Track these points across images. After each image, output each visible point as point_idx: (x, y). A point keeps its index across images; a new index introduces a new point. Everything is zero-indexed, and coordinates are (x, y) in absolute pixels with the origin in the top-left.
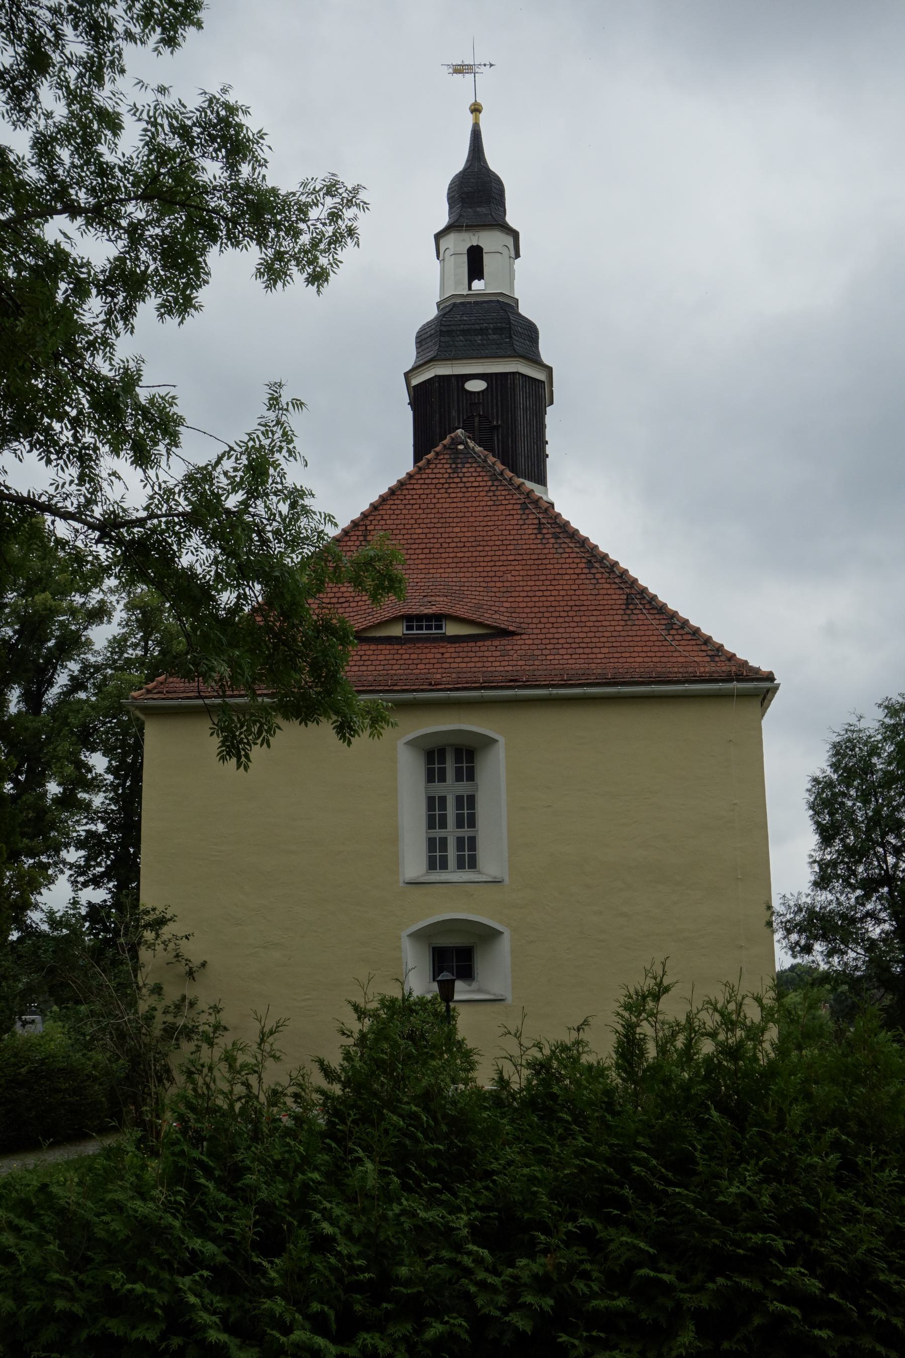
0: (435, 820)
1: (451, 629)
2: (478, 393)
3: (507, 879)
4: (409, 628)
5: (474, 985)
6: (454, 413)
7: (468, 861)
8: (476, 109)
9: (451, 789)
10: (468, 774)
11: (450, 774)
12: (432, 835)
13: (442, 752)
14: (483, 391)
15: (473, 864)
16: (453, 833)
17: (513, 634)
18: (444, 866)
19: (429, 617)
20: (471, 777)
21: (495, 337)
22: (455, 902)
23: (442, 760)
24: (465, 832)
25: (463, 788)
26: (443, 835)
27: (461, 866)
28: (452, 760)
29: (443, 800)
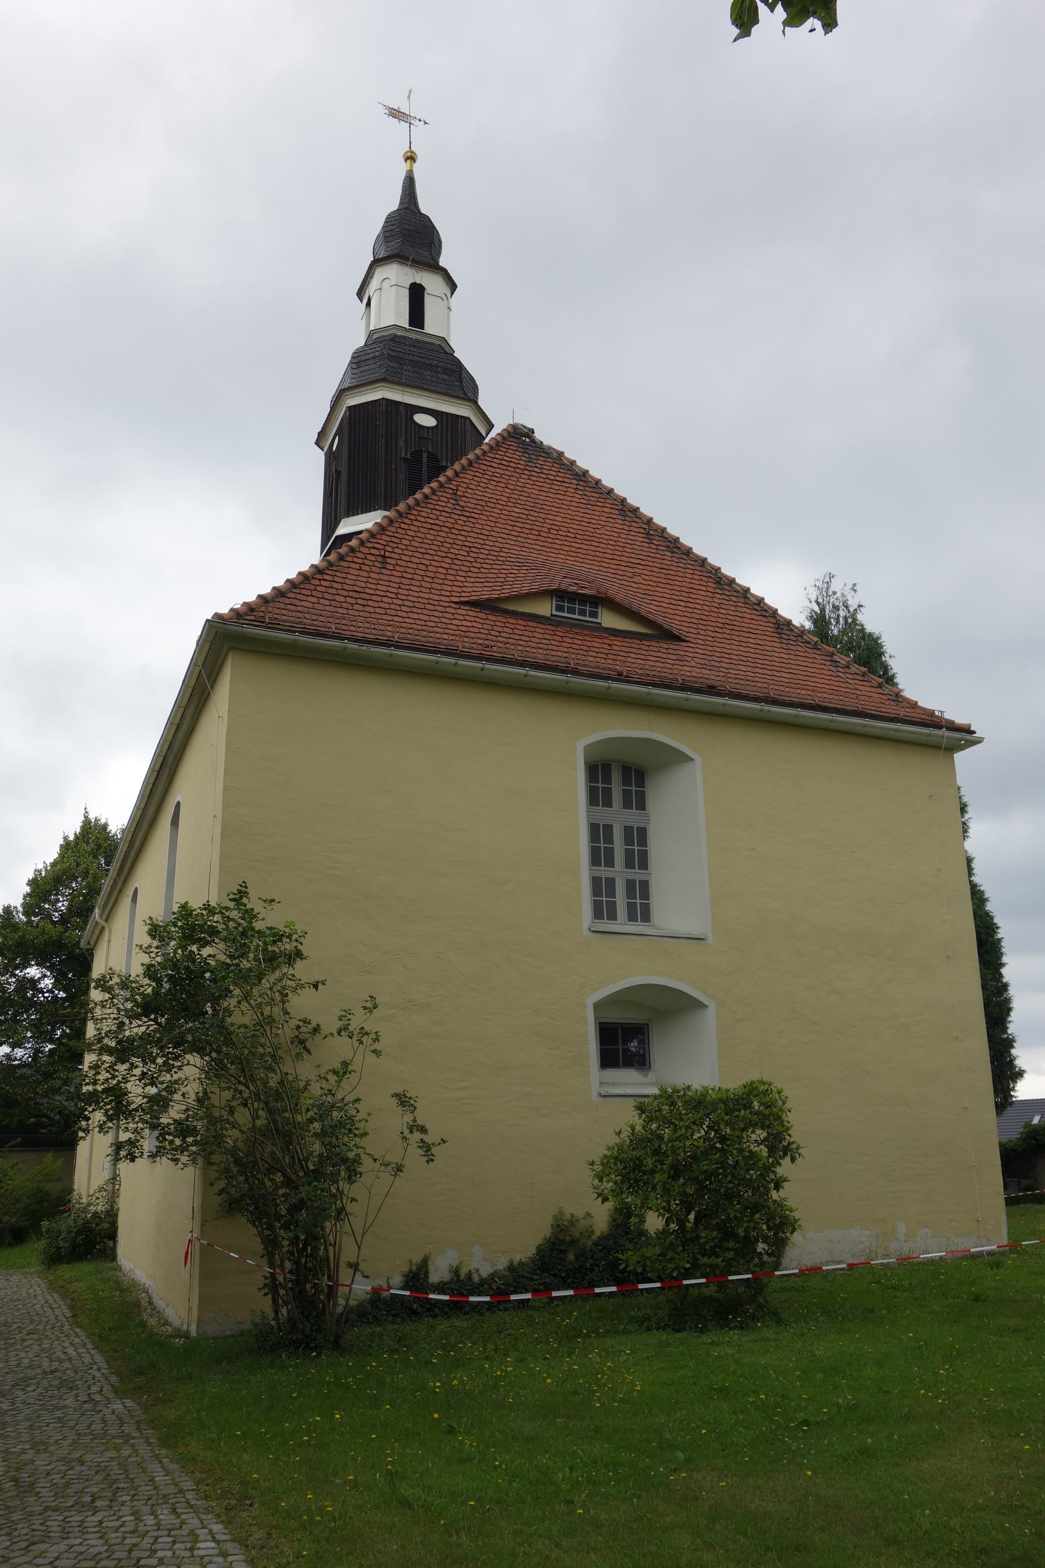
0: (600, 856)
1: (608, 620)
2: (424, 427)
3: (710, 937)
4: (559, 608)
5: (652, 1076)
6: (401, 443)
7: (641, 912)
8: (411, 158)
9: (618, 817)
10: (637, 801)
11: (617, 798)
12: (597, 874)
13: (607, 767)
14: (432, 428)
15: (646, 917)
16: (621, 877)
17: (678, 639)
18: (613, 916)
19: (583, 599)
20: (642, 805)
21: (444, 377)
22: (625, 966)
23: (607, 779)
24: (636, 874)
25: (633, 817)
26: (610, 875)
27: (632, 917)
28: (621, 778)
29: (608, 829)
